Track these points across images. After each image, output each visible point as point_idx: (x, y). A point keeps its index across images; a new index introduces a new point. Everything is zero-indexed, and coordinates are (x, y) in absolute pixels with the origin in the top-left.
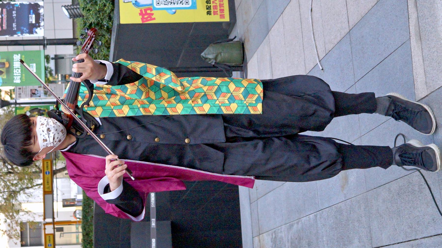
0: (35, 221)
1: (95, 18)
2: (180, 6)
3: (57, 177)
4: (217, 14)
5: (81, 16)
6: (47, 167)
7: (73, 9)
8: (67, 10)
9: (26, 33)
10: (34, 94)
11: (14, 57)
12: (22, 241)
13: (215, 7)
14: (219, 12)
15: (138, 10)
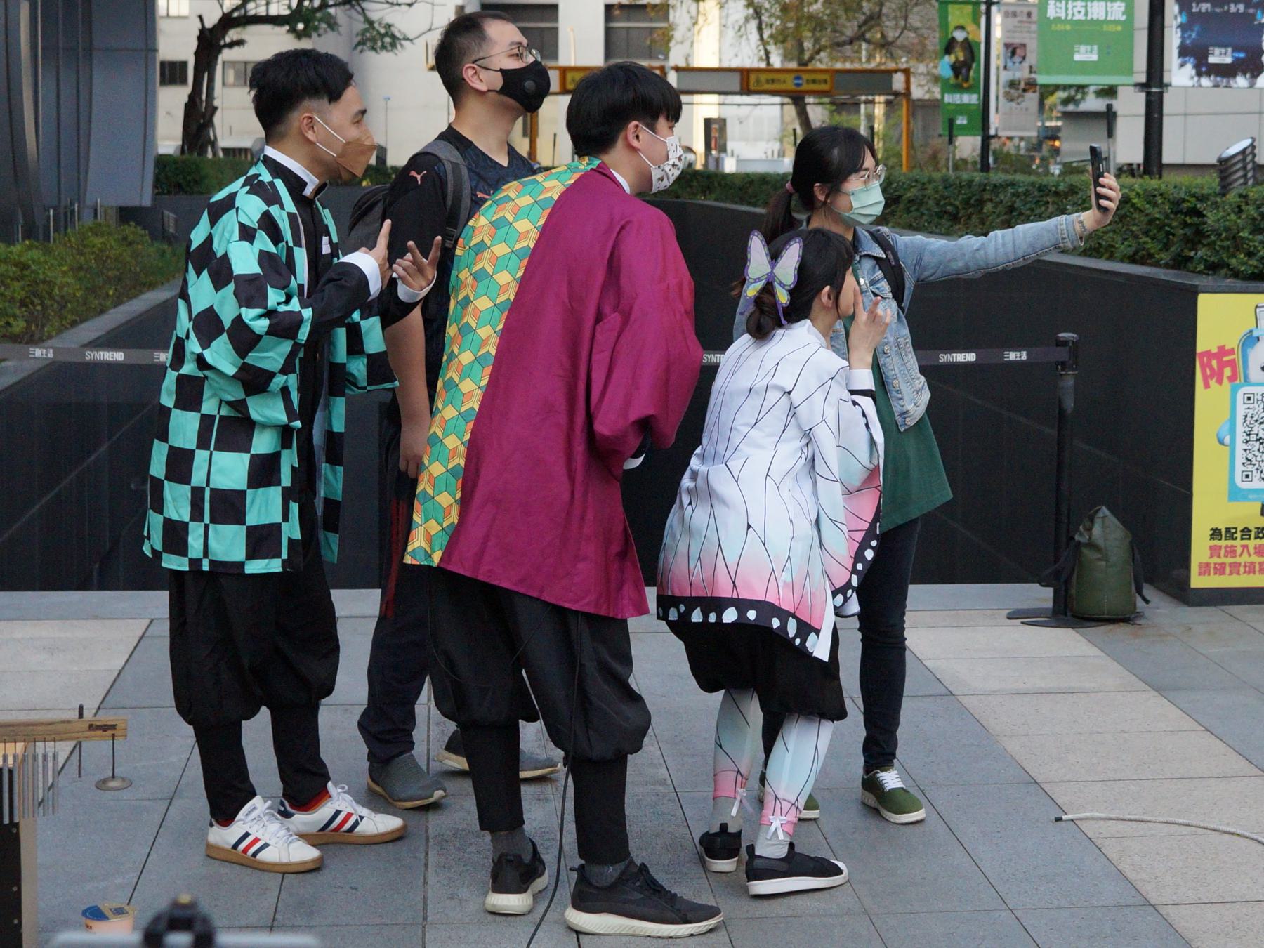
0: (671, 44)
1: (1217, 226)
2: (1240, 457)
3: (786, 107)
4: (1212, 556)
5: (1225, 188)
6: (814, 81)
7: (1244, 168)
8: (1243, 152)
9: (1182, 38)
10: (1013, 53)
11: (1118, 3)
12: (621, 6)
13: (1231, 552)
14: (1215, 560)
15: (1232, 342)
